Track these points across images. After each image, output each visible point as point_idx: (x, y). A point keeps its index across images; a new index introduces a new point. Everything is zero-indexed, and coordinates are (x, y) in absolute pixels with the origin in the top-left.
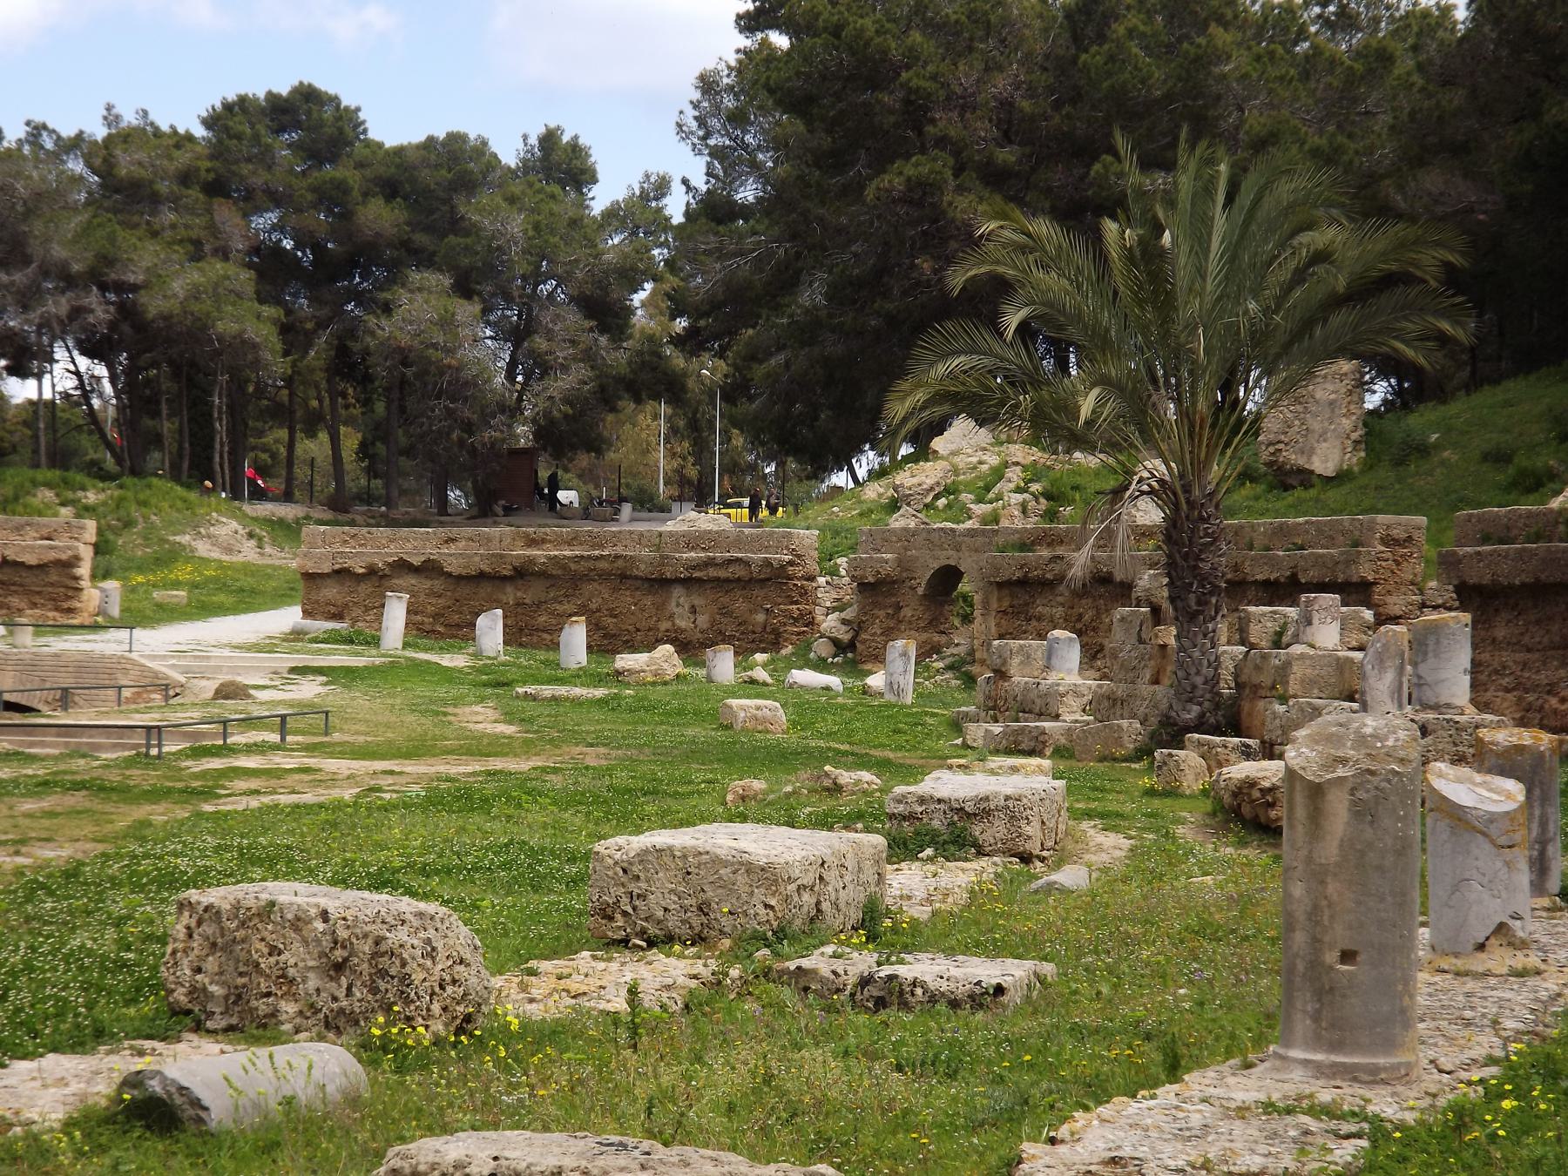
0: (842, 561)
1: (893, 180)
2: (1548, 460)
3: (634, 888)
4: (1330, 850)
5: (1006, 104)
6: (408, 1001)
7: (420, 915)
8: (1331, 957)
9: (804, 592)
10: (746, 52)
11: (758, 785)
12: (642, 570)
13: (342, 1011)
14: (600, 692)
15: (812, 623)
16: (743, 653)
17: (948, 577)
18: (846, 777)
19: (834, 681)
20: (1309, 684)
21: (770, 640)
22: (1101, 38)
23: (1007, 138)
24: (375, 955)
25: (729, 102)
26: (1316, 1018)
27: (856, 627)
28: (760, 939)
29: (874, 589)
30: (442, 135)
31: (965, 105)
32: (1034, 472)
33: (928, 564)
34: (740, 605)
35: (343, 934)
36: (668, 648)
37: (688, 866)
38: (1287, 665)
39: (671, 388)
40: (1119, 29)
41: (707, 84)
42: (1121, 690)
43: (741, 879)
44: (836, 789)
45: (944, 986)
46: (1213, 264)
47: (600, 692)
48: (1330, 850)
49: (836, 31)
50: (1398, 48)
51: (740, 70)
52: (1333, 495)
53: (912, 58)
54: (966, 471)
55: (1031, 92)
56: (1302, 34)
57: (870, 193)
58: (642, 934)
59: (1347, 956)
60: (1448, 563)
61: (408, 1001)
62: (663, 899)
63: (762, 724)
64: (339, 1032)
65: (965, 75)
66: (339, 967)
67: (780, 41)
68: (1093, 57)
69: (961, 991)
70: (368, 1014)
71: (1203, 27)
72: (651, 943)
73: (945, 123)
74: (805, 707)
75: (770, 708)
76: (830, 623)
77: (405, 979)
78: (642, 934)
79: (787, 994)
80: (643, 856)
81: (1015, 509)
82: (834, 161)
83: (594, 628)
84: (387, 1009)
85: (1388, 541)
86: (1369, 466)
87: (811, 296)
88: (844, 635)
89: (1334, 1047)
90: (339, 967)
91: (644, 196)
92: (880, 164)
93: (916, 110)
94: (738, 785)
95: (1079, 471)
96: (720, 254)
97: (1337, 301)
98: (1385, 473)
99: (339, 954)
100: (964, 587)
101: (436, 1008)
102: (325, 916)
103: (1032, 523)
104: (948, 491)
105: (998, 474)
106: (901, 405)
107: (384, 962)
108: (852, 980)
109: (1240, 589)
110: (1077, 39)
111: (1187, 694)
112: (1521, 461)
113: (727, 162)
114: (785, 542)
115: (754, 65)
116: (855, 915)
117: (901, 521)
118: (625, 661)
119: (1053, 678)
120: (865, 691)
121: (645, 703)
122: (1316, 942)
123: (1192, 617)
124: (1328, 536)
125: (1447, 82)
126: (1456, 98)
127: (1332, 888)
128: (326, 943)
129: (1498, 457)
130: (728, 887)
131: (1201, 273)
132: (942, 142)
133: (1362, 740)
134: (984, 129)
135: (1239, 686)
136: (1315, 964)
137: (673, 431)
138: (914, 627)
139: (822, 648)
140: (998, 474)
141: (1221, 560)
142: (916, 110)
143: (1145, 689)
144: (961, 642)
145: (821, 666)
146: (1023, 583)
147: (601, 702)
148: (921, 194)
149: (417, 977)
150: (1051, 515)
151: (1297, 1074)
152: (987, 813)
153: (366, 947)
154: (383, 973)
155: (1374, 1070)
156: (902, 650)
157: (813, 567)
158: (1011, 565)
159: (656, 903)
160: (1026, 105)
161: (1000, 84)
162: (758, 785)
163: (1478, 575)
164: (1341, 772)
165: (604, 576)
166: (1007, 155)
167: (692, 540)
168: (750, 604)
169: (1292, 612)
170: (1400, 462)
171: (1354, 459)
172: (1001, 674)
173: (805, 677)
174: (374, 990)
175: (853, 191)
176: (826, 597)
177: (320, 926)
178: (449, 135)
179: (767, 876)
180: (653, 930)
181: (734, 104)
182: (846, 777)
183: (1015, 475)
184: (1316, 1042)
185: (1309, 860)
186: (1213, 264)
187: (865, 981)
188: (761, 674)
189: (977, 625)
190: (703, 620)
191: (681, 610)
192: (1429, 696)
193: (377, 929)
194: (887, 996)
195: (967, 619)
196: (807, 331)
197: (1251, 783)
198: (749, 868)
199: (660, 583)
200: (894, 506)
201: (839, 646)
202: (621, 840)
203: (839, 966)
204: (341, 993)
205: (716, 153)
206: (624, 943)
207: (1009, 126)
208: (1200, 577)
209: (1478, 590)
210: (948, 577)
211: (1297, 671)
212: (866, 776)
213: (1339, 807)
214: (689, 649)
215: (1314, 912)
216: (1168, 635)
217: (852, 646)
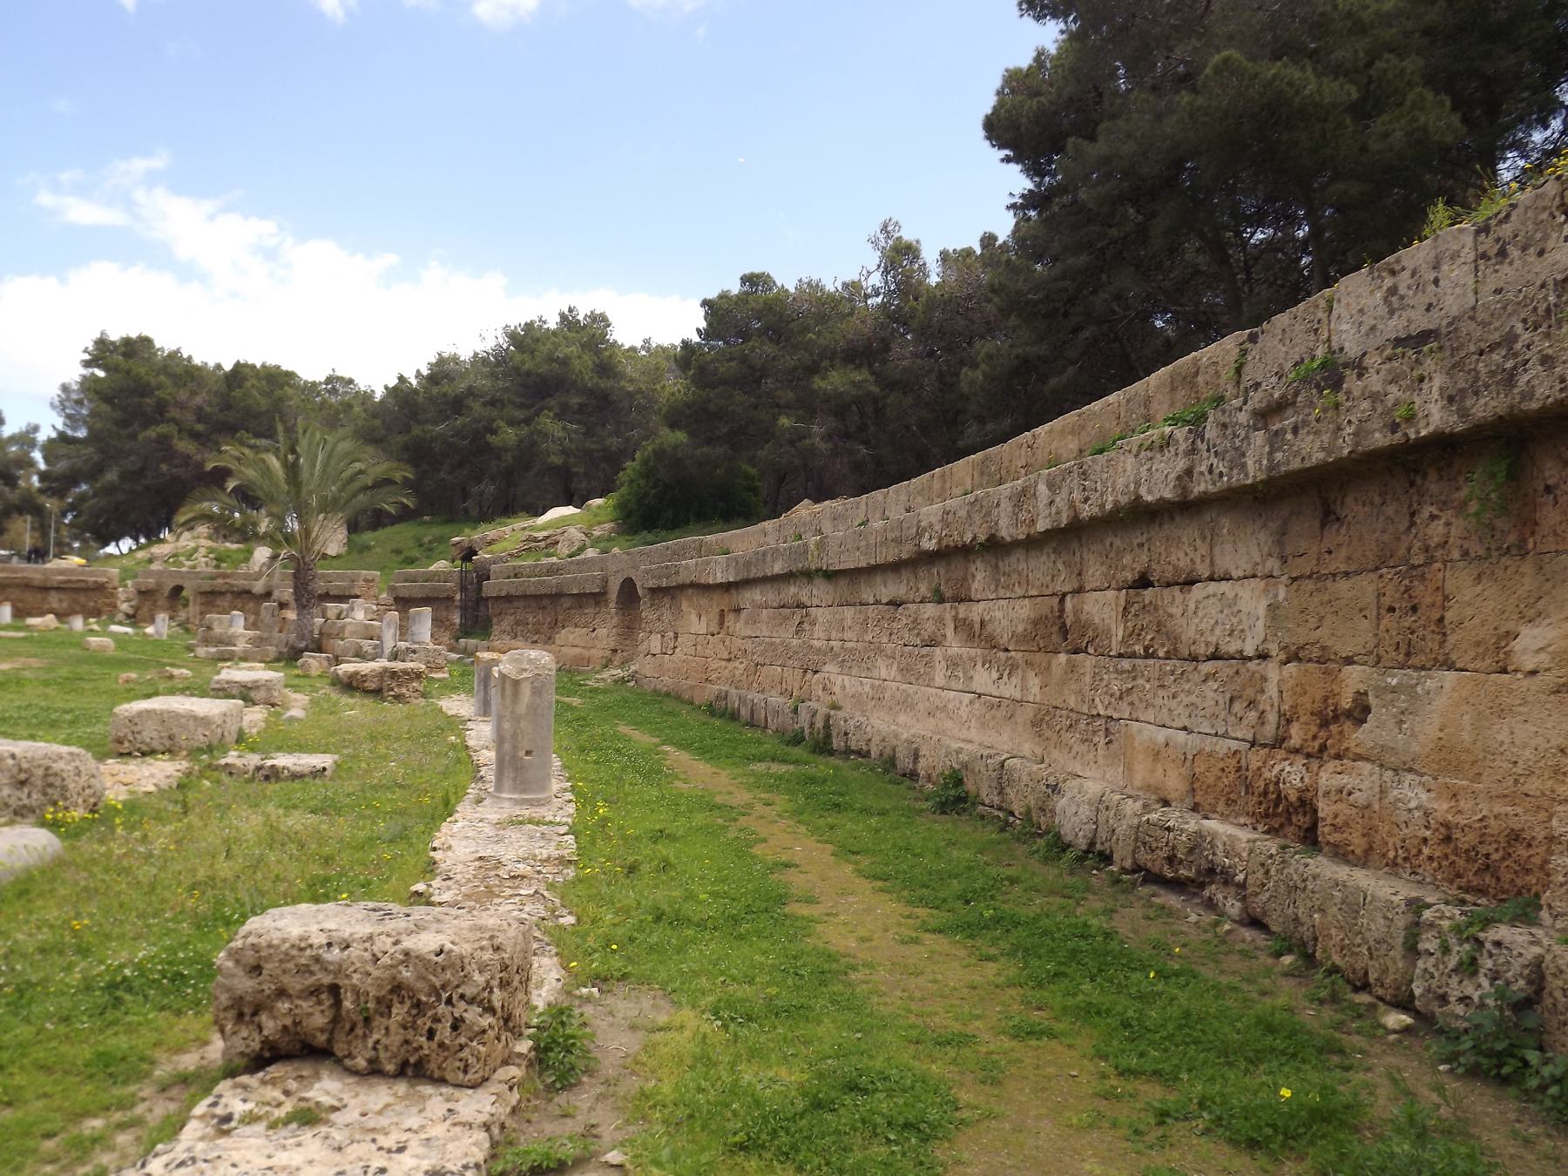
0: (129, 582)
1: (152, 432)
2: (416, 553)
3: (135, 729)
4: (522, 708)
5: (200, 408)
6: (66, 799)
7: (71, 754)
8: (522, 753)
9: (112, 594)
10: (84, 377)
11: (134, 675)
12: (36, 583)
13: (24, 806)
14: (21, 634)
15: (115, 607)
16: (86, 618)
17: (178, 590)
18: (176, 672)
19: (129, 630)
20: (353, 634)
21: (96, 613)
22: (240, 387)
23: (199, 421)
24: (46, 776)
25: (74, 396)
26: (514, 780)
27: (137, 609)
28: (200, 750)
29: (145, 594)
30: (228, 367)
31: (182, 406)
32: (211, 550)
33: (170, 584)
34: (82, 599)
35: (25, 765)
36: (51, 616)
37: (162, 718)
38: (343, 627)
39: (38, 511)
40: (248, 384)
41: (65, 388)
42: (265, 635)
43: (191, 723)
44: (171, 677)
45: (298, 769)
46: (317, 471)
47: (21, 634)
48: (522, 708)
49: (128, 372)
50: (354, 403)
51: (82, 384)
52: (334, 563)
53: (160, 387)
54: (186, 548)
55: (210, 404)
56: (319, 394)
57: (140, 437)
58: (139, 750)
59: (528, 753)
60: (392, 589)
61: (66, 799)
62: (150, 733)
63: (103, 648)
64: (23, 816)
65: (183, 395)
66: (23, 783)
67: (101, 374)
68: (237, 393)
69: (306, 770)
70: (41, 807)
71: (282, 387)
72: (144, 754)
73: (174, 413)
74: (120, 640)
75: (106, 641)
76: (124, 607)
77: (64, 788)
78: (139, 750)
79: (224, 777)
80: (140, 714)
81: (202, 562)
82: (124, 423)
83: (14, 607)
84: (55, 804)
85: (366, 580)
86: (348, 553)
87: (111, 476)
88: (131, 612)
89: (523, 791)
90: (23, 783)
91: (28, 432)
92: (145, 426)
93: (161, 407)
94: (124, 675)
95: (228, 550)
96: (68, 457)
97: (365, 488)
98: (355, 556)
99: (23, 776)
100: (184, 593)
101: (80, 801)
102: (13, 756)
103: (210, 569)
104: (175, 555)
105: (196, 550)
106: (181, 518)
107: (51, 780)
108: (251, 768)
109: (327, 597)
110: (229, 386)
111: (301, 637)
112: (407, 553)
113: (72, 420)
114: (104, 573)
115: (88, 384)
116: (235, 736)
117: (155, 567)
118: (31, 621)
119: (232, 630)
120: (145, 634)
121: (42, 640)
122: (515, 748)
123: (304, 607)
124: (340, 577)
125: (374, 417)
126: (377, 422)
127: (523, 724)
128: (15, 770)
129: (398, 552)
130: (185, 727)
131: (312, 475)
132: (173, 420)
133: (530, 661)
134: (190, 417)
135: (321, 634)
136: (514, 757)
137: (33, 528)
138: (165, 610)
139: (120, 617)
140: (196, 550)
141: (320, 586)
142: (161, 407)
143: (276, 634)
144: (182, 615)
145: (120, 623)
146: (212, 592)
147: (24, 639)
148: (163, 440)
149: (72, 786)
150: (217, 567)
151: (506, 804)
152: (257, 688)
153: (40, 772)
154: (51, 785)
155: (539, 800)
156: (162, 617)
157: (116, 584)
158: (207, 586)
159: (146, 736)
160: (208, 409)
161: (198, 400)
162: (134, 675)
163: (404, 594)
164: (525, 675)
165: (18, 586)
166: (200, 427)
167: (62, 572)
168: (88, 598)
169: (345, 606)
170: (361, 552)
171: (343, 550)
172: (209, 628)
173: (115, 628)
174: (45, 794)
175: (133, 436)
176: (122, 597)
177: (10, 762)
178: (238, 364)
179: (205, 721)
180: (144, 748)
181: (67, 401)
182: (176, 672)
183: (202, 551)
184: (514, 790)
185: (513, 712)
186: (317, 471)
187: (259, 769)
188: (95, 627)
189: (191, 608)
190: (65, 605)
191: (54, 599)
192: (416, 639)
193: (47, 762)
194: (273, 774)
195: (186, 606)
196: (110, 490)
197: (357, 673)
198: (195, 718)
199: (45, 589)
200: (150, 561)
201: (128, 616)
202: (126, 706)
203: (244, 761)
204: (24, 796)
205: (68, 417)
206: (129, 754)
207: (201, 416)
208: (307, 595)
209: (402, 599)
210: (178, 590)
211: (348, 629)
212: (185, 671)
213: (526, 690)
214: (61, 616)
215: (514, 736)
216: (291, 615)
217: (133, 616)
